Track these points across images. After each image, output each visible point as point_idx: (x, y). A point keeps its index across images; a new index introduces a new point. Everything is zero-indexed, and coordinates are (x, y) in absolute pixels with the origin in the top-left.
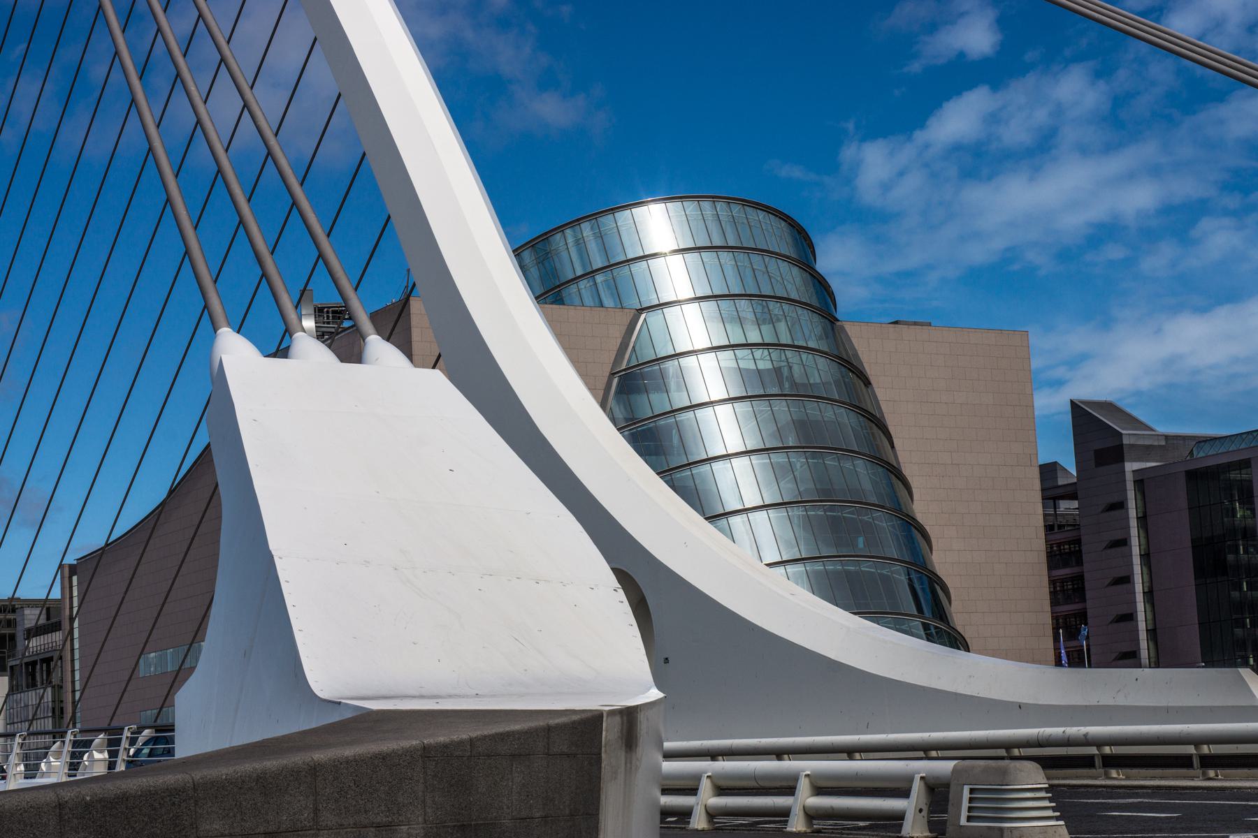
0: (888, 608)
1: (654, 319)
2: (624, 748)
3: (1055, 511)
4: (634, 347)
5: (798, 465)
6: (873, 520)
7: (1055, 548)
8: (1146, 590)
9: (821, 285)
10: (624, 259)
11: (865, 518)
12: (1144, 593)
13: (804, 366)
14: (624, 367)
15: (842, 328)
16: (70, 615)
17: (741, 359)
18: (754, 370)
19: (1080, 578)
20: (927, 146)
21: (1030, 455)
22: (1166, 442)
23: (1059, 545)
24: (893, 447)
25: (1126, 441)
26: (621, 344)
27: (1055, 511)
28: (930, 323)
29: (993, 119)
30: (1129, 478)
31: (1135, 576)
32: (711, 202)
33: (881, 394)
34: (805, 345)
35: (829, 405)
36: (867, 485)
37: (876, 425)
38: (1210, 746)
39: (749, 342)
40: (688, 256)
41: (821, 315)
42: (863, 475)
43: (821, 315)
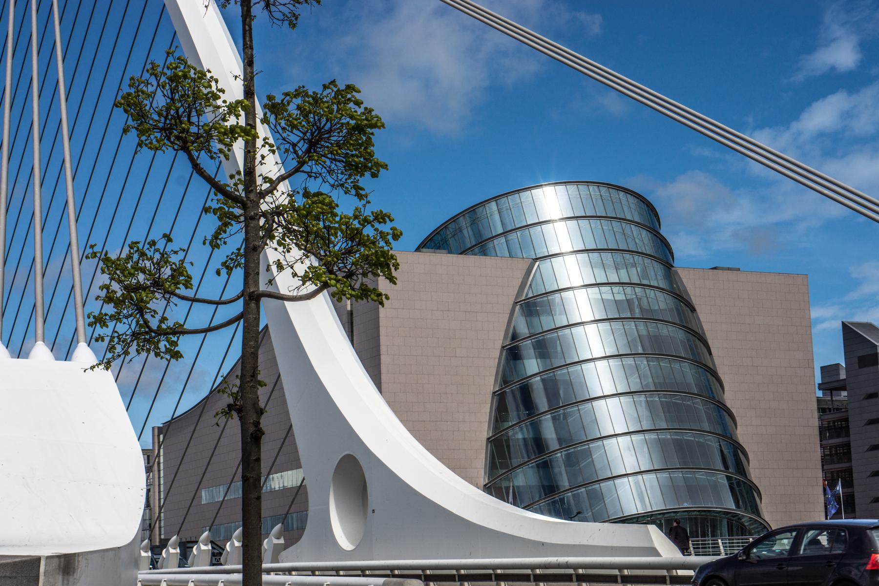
0: (702, 465)
1: (545, 265)
2: (61, 573)
3: (832, 398)
4: (530, 285)
5: (642, 366)
6: (693, 404)
7: (831, 424)
9: (663, 244)
10: (525, 224)
11: (688, 403)
13: (647, 298)
14: (523, 298)
15: (676, 272)
17: (604, 293)
18: (612, 300)
19: (848, 445)
20: (800, 133)
23: (834, 422)
24: (710, 354)
27: (832, 398)
29: (847, 115)
32: (586, 186)
33: (703, 317)
34: (649, 284)
35: (665, 325)
36: (690, 380)
37: (698, 338)
38: (629, 570)
41: (661, 263)
42: (687, 373)
43: (661, 263)
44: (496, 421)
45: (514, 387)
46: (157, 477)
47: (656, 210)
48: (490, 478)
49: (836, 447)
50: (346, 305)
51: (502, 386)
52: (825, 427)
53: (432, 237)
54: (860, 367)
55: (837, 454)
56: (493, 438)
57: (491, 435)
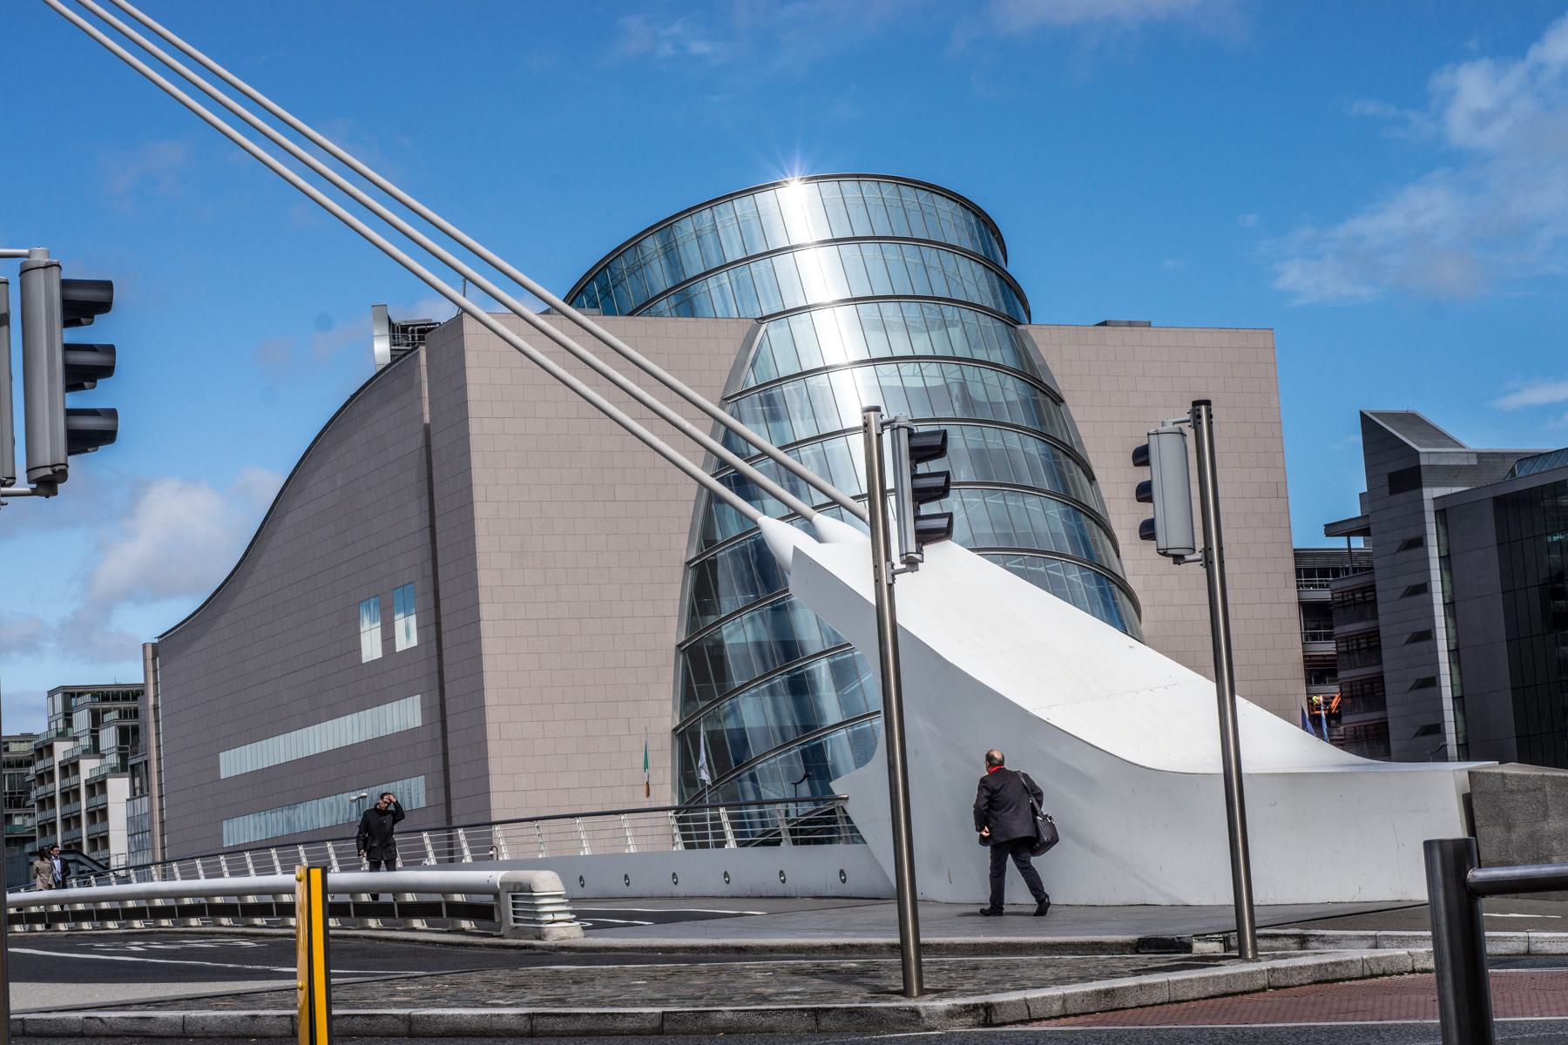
8: (1452, 648)
10: (764, 250)
12: (1449, 651)
16: (154, 705)
18: (898, 387)
20: (1541, 67)
21: (1277, 483)
22: (1479, 462)
25: (1424, 461)
26: (735, 362)
28: (1150, 322)
30: (1429, 507)
31: (1438, 631)
35: (998, 430)
39: (895, 355)
40: (844, 248)
44: (692, 613)
45: (723, 553)
46: (154, 733)
47: (993, 222)
48: (683, 716)
49: (1358, 636)
50: (423, 414)
51: (702, 550)
52: (1339, 602)
53: (584, 286)
54: (1392, 493)
55: (1359, 650)
56: (688, 644)
57: (683, 639)
